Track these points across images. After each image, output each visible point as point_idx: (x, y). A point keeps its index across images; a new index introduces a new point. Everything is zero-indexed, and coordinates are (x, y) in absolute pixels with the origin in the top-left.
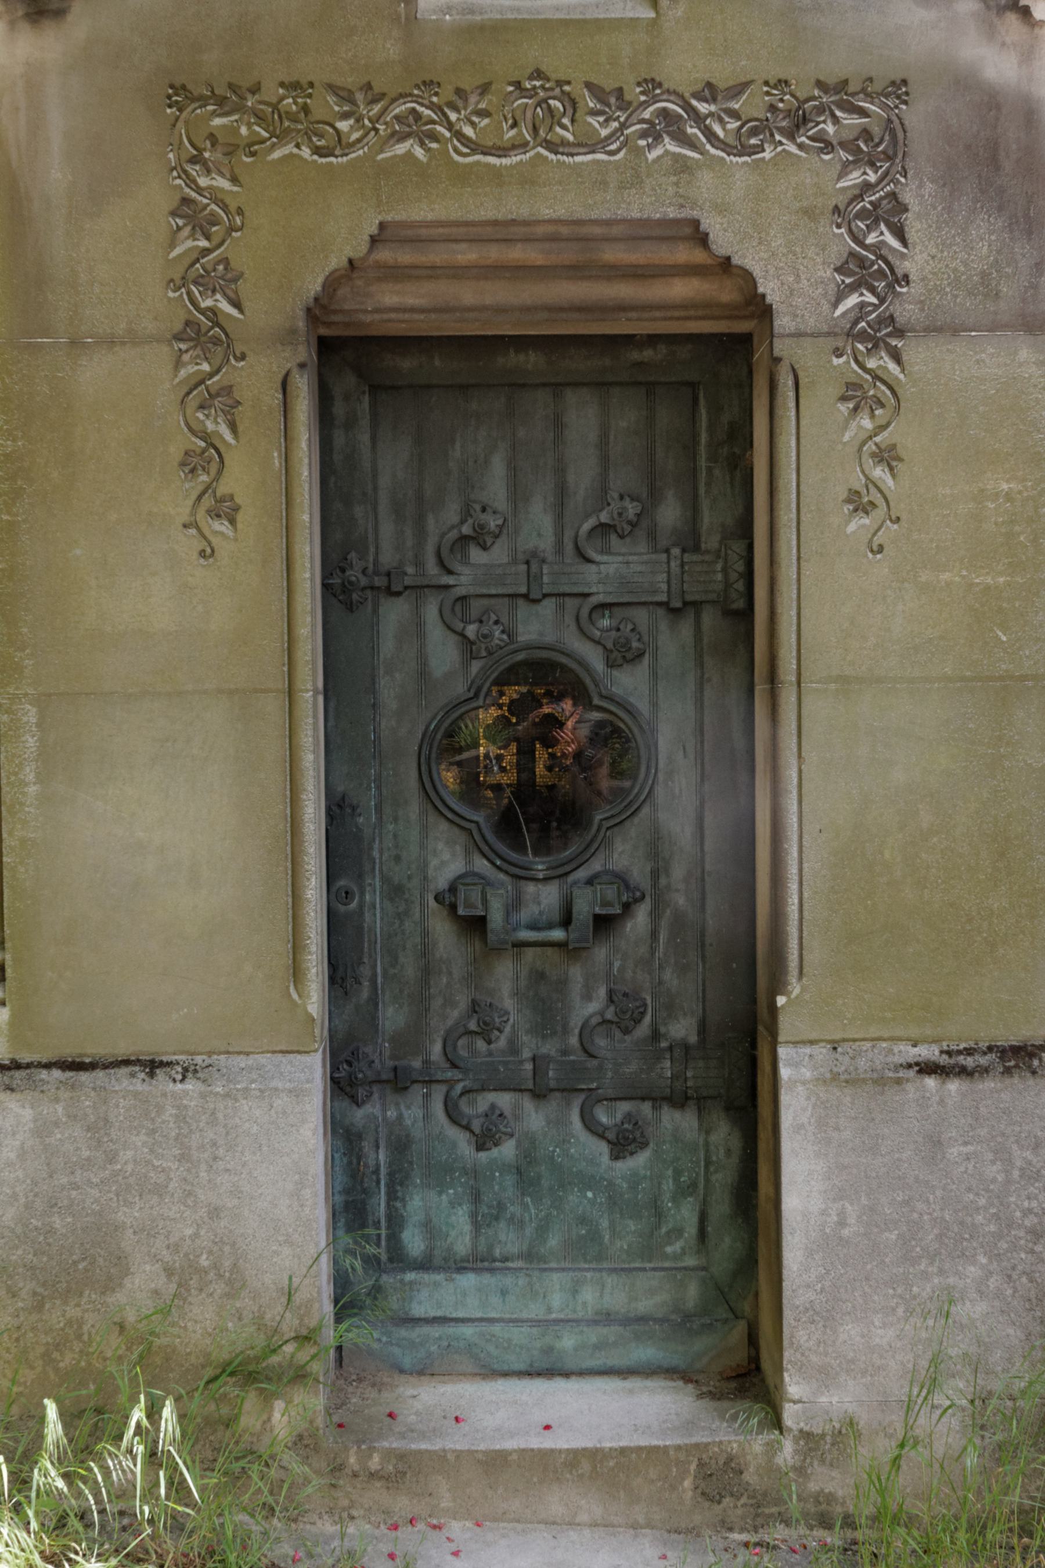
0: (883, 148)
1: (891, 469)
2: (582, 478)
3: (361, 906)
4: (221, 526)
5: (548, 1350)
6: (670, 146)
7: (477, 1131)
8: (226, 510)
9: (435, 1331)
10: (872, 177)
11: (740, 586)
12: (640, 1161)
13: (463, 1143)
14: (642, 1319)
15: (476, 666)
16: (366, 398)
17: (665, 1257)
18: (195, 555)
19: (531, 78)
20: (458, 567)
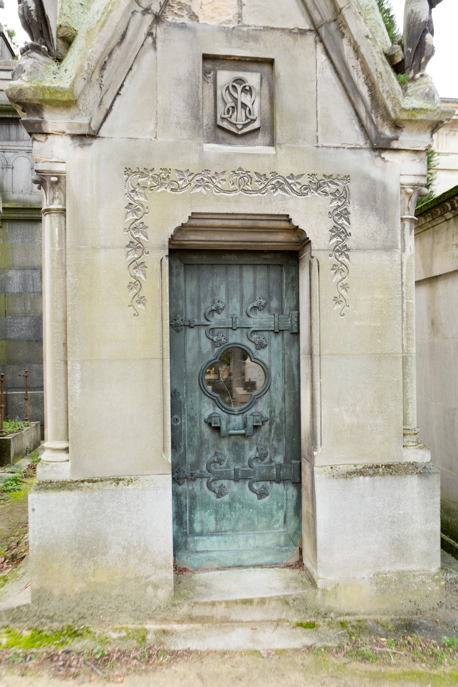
0: (342, 196)
1: (346, 291)
2: (248, 291)
3: (181, 424)
4: (140, 306)
5: (239, 560)
6: (279, 191)
7: (217, 492)
8: (142, 300)
9: (204, 555)
10: (340, 204)
11: (296, 325)
12: (266, 500)
13: (213, 496)
14: (267, 548)
15: (216, 349)
16: (183, 268)
17: (274, 529)
18: (132, 315)
19: (238, 170)
20: (211, 319)
